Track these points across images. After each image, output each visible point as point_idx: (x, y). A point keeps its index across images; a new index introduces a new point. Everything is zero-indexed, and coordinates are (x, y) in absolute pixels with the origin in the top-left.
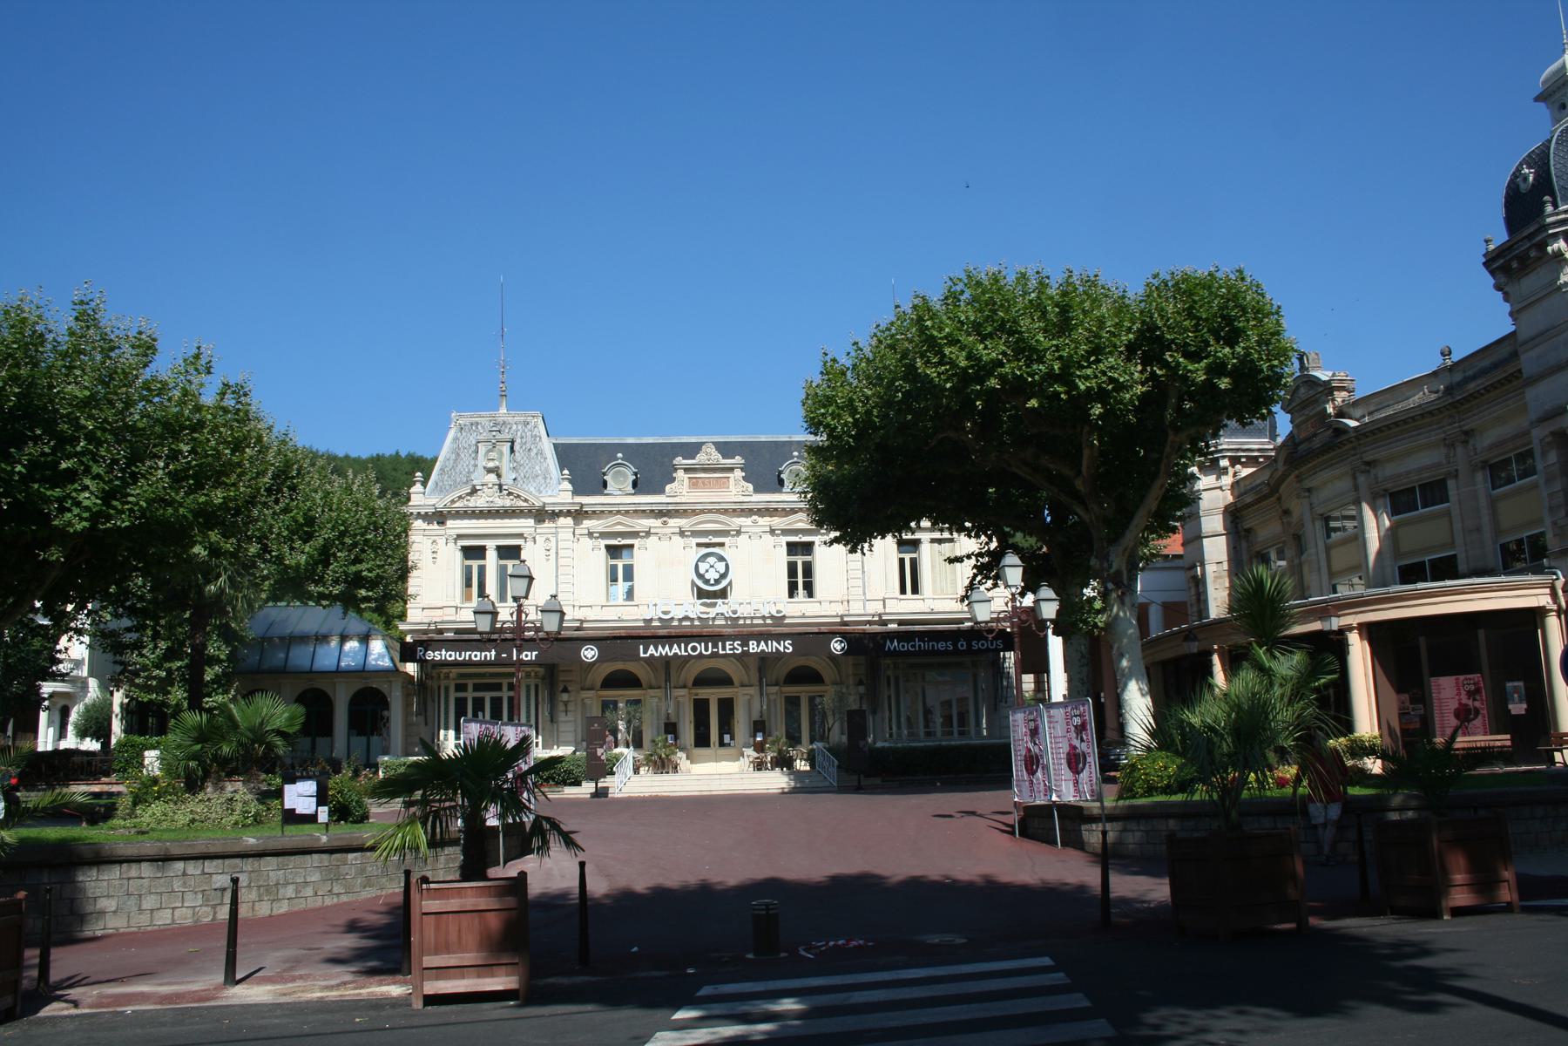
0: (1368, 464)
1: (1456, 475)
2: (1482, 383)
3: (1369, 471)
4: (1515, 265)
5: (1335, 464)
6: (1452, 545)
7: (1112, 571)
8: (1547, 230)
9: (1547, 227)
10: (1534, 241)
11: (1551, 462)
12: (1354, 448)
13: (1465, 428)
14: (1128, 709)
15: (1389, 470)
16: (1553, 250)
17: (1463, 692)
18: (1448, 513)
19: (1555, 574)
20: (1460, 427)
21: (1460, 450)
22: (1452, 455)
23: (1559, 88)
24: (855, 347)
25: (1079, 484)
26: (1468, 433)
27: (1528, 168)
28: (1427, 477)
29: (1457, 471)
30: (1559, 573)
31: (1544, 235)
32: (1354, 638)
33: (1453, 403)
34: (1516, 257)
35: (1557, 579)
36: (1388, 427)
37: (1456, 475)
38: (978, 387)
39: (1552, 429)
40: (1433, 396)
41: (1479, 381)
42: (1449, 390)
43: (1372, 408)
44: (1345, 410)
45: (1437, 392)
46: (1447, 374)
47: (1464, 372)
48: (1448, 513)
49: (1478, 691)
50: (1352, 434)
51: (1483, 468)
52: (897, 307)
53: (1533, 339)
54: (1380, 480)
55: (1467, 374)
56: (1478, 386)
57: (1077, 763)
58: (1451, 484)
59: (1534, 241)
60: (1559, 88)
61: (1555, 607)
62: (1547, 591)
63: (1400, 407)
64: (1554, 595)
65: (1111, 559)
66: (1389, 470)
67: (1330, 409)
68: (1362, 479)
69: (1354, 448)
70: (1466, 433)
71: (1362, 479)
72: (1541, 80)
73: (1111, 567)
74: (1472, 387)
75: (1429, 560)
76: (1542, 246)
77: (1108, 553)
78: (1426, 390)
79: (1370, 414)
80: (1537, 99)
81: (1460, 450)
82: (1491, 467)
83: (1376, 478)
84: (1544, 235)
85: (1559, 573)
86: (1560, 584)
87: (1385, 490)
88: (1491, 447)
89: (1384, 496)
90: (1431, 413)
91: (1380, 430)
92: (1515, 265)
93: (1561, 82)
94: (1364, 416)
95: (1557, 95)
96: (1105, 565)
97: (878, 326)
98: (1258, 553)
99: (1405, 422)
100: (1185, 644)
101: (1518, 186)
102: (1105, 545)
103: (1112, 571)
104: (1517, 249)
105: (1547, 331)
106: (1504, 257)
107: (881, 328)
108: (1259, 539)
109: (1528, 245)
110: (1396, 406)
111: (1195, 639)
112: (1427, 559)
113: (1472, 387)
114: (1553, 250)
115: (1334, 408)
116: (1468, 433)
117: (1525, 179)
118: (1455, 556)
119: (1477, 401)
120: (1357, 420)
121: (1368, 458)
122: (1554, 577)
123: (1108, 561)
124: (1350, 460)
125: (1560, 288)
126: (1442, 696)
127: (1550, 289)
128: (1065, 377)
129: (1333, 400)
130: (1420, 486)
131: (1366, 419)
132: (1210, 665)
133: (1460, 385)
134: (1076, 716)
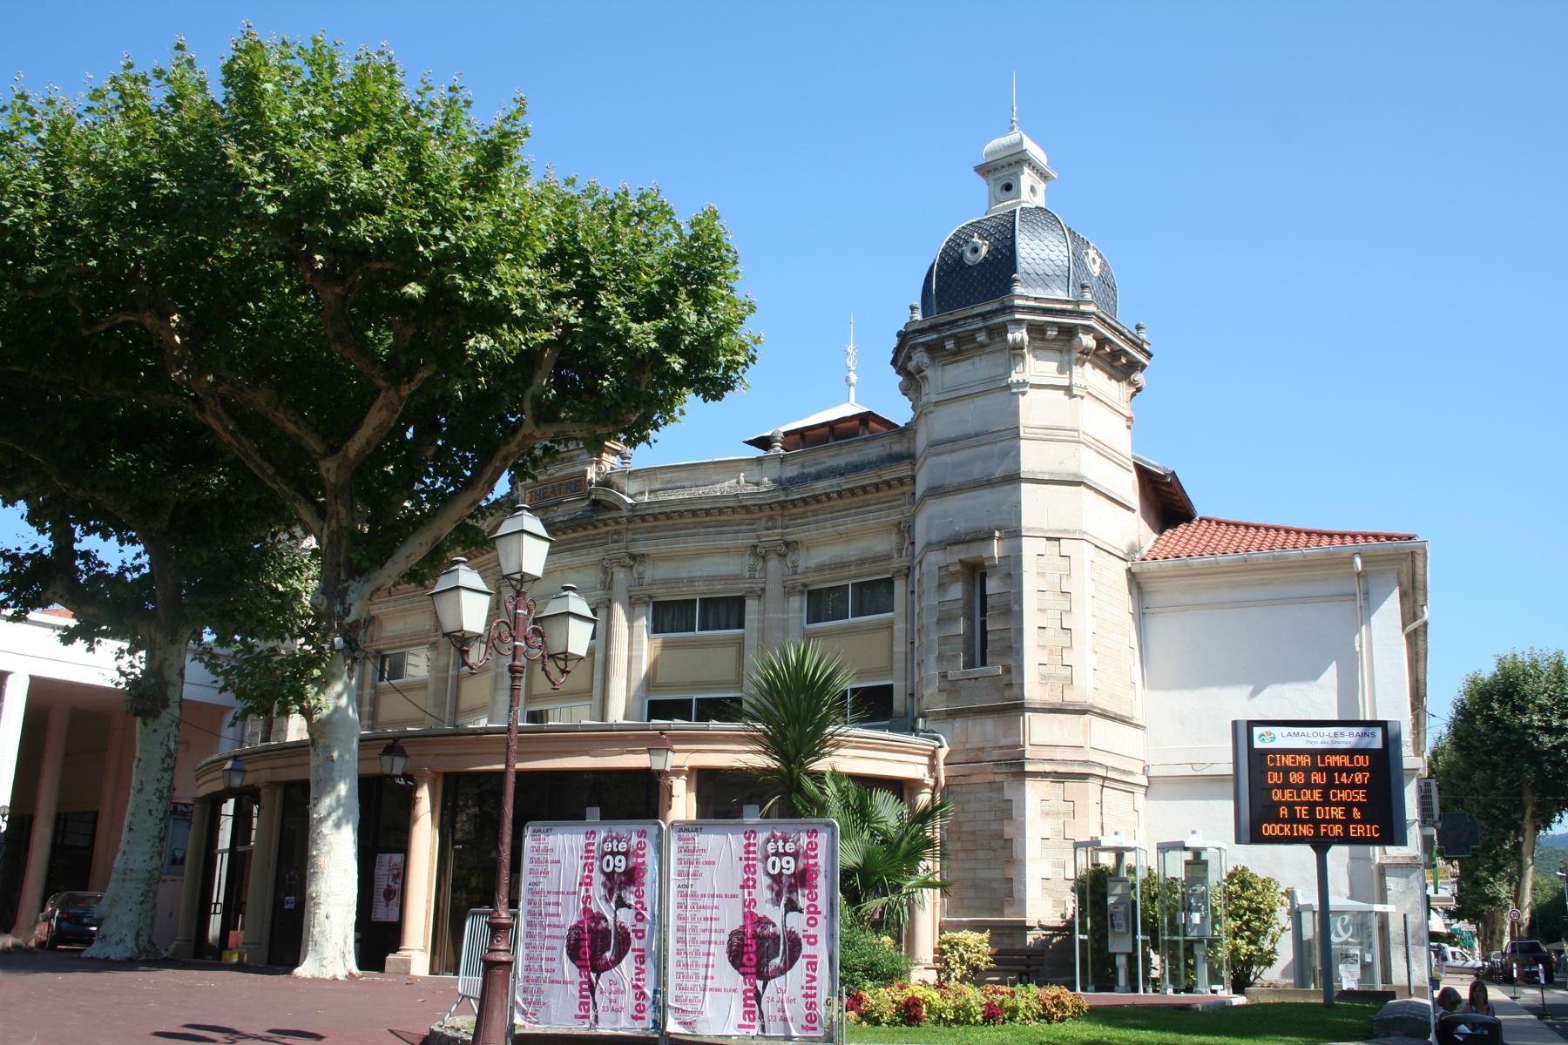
0: (633, 557)
1: (761, 594)
2: (839, 485)
3: (631, 567)
4: (950, 345)
5: (582, 548)
6: (739, 683)
7: (349, 620)
8: (1012, 312)
9: (1013, 309)
10: (991, 323)
11: (949, 598)
12: (617, 532)
13: (789, 538)
14: (325, 849)
15: (662, 571)
16: (1014, 340)
17: (763, 881)
18: (740, 643)
19: (937, 739)
20: (783, 534)
21: (773, 563)
22: (759, 568)
23: (1009, 165)
24: (19, 102)
25: (329, 469)
26: (790, 545)
27: (981, 237)
28: (719, 590)
29: (763, 590)
30: (942, 737)
31: (1009, 318)
32: (679, 786)
33: (786, 501)
34: (954, 336)
35: (941, 747)
36: (681, 514)
37: (761, 594)
38: (330, 231)
39: (963, 556)
40: (751, 489)
41: (834, 481)
42: (783, 484)
43: (657, 486)
44: (614, 479)
45: (757, 484)
46: (778, 465)
47: (803, 466)
48: (889, 626)
49: (803, 878)
50: (626, 513)
51: (802, 593)
52: (179, 47)
53: (952, 441)
54: (646, 581)
55: (806, 470)
56: (832, 486)
57: (763, 957)
58: (751, 606)
59: (991, 323)
60: (1009, 165)
61: (931, 782)
62: (926, 760)
63: (700, 491)
64: (932, 768)
65: (348, 601)
66: (662, 571)
67: (592, 473)
68: (620, 575)
69: (617, 532)
70: (787, 544)
71: (620, 575)
72: (988, 147)
73: (347, 612)
74: (821, 486)
75: (697, 699)
76: (1002, 330)
77: (346, 590)
78: (742, 479)
79: (651, 492)
80: (978, 169)
81: (773, 563)
82: (810, 593)
83: (641, 577)
84: (1009, 318)
85: (942, 737)
86: (942, 754)
87: (650, 597)
88: (821, 568)
89: (647, 604)
90: (747, 509)
91: (668, 516)
92: (950, 345)
93: (1015, 158)
94: (642, 493)
95: (1004, 173)
96: (338, 608)
97: (130, 66)
98: (378, 652)
99: (707, 512)
100: (387, 759)
101: (961, 255)
102: (343, 577)
103: (349, 620)
104: (959, 326)
105: (976, 435)
106: (939, 332)
107: (131, 72)
108: (384, 634)
109: (980, 325)
110: (693, 490)
111: (402, 754)
112: (695, 697)
113: (821, 486)
114: (1014, 340)
115: (597, 474)
116: (790, 545)
117: (975, 250)
118: (891, 686)
119: (820, 506)
120: (631, 497)
121: (637, 549)
122: (937, 744)
123: (343, 603)
124: (606, 547)
125: (1008, 387)
126: (699, 886)
127: (992, 386)
128: (481, 262)
129: (598, 463)
130: (700, 599)
131: (646, 499)
132: (409, 802)
133: (792, 481)
134: (613, 854)
